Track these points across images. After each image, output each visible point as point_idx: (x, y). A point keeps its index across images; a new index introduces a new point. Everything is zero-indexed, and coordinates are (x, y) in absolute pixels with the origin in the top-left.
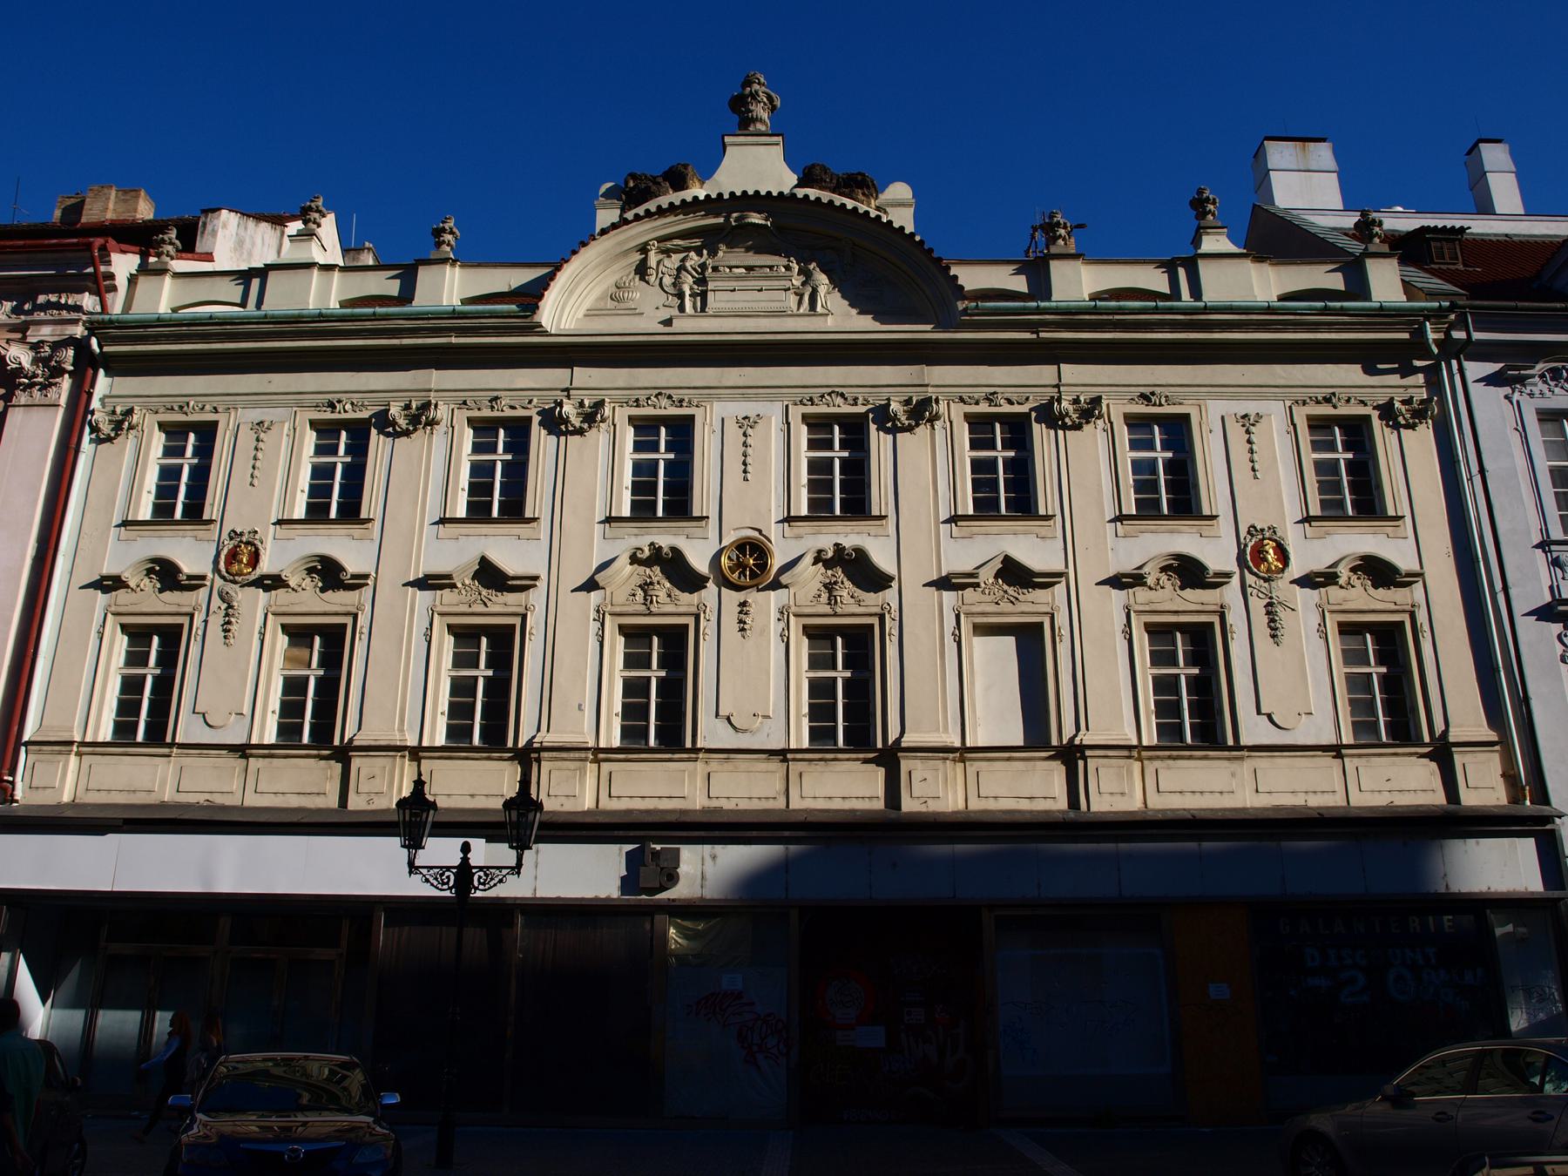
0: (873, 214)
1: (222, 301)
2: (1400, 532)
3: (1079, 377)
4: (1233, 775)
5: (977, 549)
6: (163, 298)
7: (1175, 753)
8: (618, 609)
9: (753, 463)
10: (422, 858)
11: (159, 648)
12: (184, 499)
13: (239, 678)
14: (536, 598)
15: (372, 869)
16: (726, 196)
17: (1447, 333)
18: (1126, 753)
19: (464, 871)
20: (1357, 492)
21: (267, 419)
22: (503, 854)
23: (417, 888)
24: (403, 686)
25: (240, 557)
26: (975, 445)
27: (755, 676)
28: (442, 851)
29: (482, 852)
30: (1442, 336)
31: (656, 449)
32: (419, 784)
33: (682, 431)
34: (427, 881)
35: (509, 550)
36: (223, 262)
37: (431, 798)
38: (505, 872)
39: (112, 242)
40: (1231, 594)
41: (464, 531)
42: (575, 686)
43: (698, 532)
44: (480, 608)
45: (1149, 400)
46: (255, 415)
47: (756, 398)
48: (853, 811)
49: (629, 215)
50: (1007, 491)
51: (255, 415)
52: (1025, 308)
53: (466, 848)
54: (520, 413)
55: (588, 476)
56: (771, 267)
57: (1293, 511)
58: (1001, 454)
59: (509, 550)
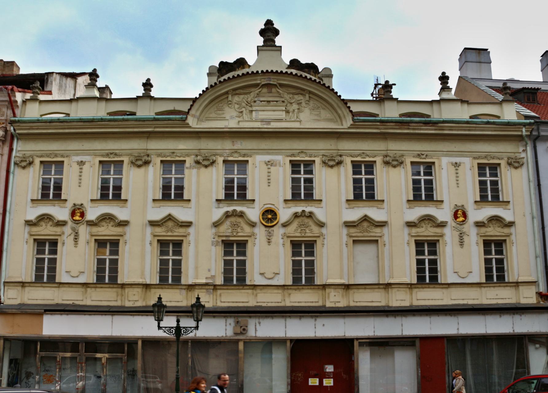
0: (318, 80)
1: (56, 113)
2: (508, 207)
5: (355, 214)
6: (32, 112)
8: (221, 234)
9: (269, 180)
10: (162, 324)
11: (46, 247)
12: (51, 192)
13: (76, 260)
14: (191, 230)
15: (145, 328)
16: (260, 72)
17: (531, 132)
18: (406, 286)
19: (178, 329)
20: (490, 193)
21: (84, 160)
22: (191, 323)
23: (161, 334)
24: (138, 262)
26: (413, 175)
27: (268, 259)
28: (170, 321)
29: (187, 322)
30: (529, 133)
32: (160, 299)
33: (429, 168)
34: (165, 332)
35: (180, 212)
36: (55, 96)
37: (203, 303)
38: (192, 329)
39: (15, 88)
40: (67, 230)
41: (162, 204)
42: (202, 261)
43: (251, 206)
44: (169, 234)
46: (79, 158)
49: (222, 79)
50: (364, 192)
51: (268, 158)
52: (375, 120)
54: (312, 159)
55: (205, 185)
56: (277, 101)
57: (471, 201)
59: (180, 212)
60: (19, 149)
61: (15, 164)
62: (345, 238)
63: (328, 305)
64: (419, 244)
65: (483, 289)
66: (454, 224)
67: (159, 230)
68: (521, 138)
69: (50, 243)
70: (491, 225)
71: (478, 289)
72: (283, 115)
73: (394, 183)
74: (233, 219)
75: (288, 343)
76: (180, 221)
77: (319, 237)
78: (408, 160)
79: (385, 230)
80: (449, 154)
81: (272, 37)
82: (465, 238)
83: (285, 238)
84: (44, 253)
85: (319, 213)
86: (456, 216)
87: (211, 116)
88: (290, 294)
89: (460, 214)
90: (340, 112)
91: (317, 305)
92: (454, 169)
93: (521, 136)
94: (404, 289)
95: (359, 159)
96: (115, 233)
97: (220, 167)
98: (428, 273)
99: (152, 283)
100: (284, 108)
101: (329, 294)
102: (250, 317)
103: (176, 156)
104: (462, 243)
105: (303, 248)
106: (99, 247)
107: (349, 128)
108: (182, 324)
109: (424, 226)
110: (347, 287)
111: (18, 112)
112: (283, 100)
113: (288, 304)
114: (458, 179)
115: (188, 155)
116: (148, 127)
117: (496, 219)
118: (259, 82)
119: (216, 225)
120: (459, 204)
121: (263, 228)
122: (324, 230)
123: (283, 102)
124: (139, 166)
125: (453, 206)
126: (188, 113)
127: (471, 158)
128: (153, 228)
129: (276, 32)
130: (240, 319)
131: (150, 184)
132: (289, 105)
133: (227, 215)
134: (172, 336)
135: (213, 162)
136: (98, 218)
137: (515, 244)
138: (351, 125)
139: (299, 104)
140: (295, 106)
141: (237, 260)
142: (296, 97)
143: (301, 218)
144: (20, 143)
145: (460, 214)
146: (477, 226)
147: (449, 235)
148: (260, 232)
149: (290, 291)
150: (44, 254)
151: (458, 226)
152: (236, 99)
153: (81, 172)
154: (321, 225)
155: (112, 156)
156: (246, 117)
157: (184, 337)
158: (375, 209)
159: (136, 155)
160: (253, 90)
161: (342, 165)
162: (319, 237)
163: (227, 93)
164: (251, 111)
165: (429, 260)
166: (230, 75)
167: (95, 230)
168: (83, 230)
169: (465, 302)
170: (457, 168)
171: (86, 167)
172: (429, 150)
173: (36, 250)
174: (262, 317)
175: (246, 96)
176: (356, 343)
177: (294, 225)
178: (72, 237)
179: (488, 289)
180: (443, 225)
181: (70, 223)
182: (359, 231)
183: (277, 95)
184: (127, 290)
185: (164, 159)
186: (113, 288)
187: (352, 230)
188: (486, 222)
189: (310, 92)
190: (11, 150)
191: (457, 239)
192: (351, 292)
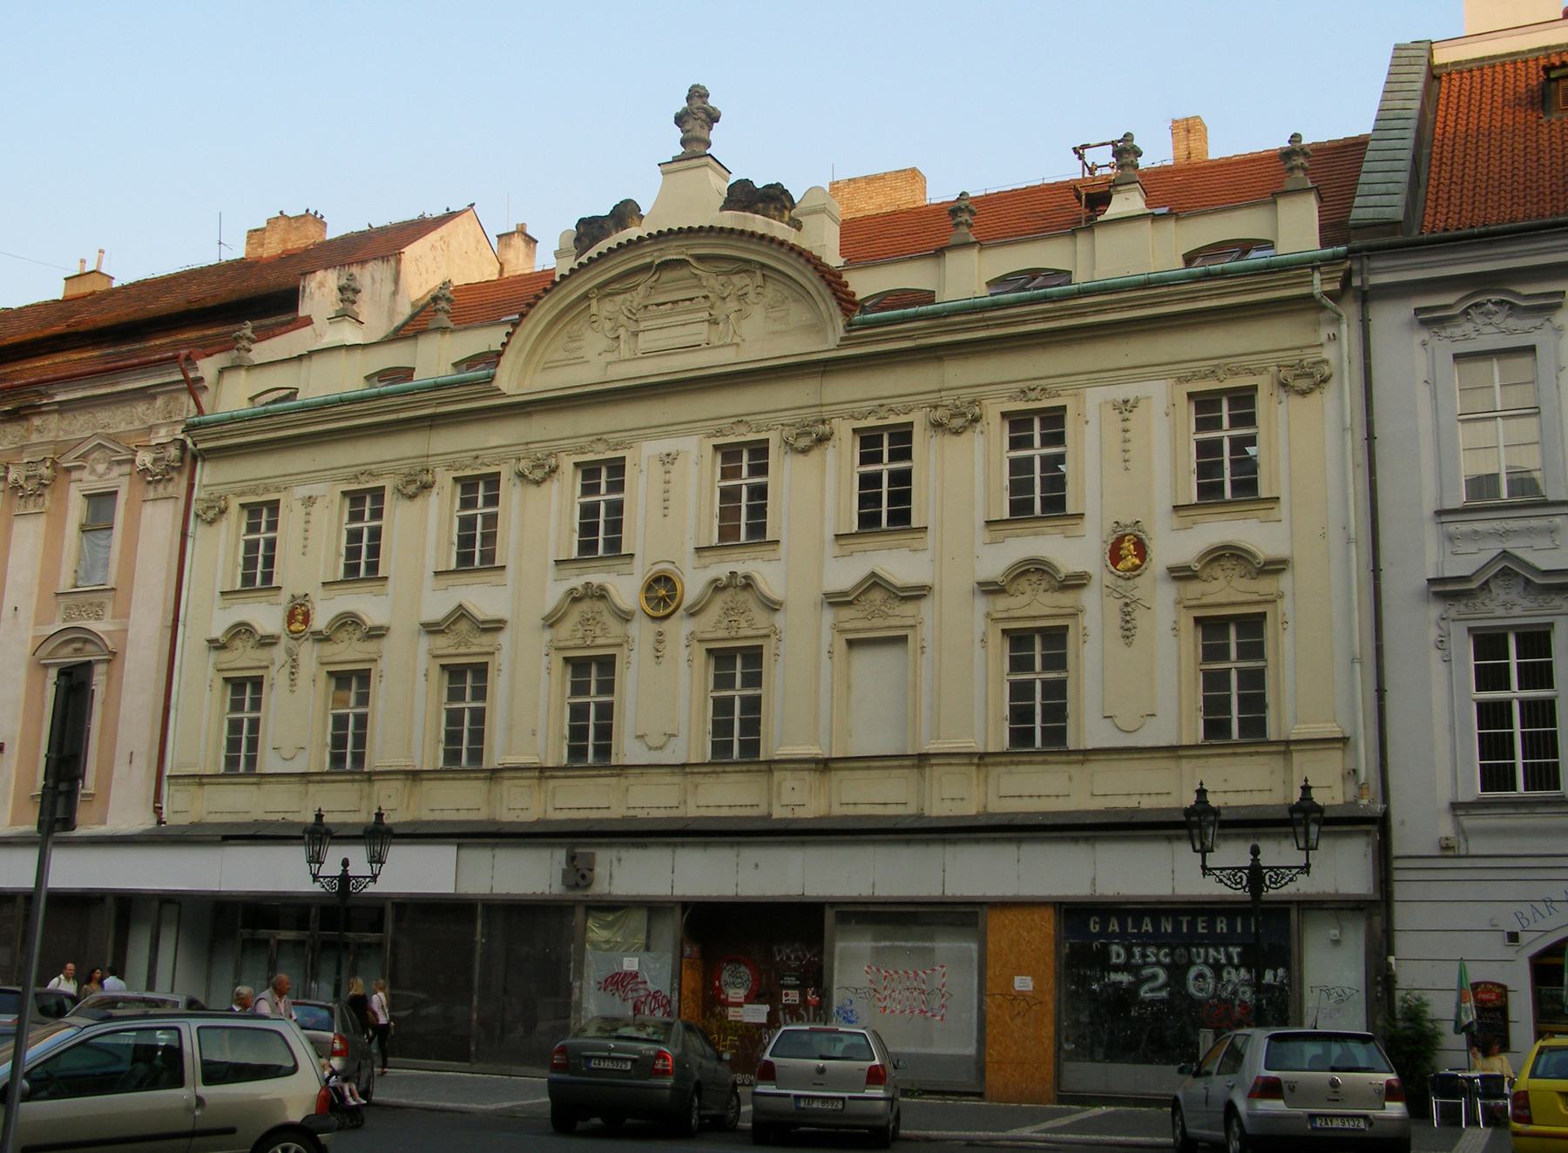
2: (1274, 514)
3: (959, 375)
4: (1070, 779)
7: (1253, 749)
8: (562, 644)
10: (1213, 860)
14: (503, 638)
15: (283, 872)
18: (966, 761)
19: (1256, 875)
20: (1226, 477)
23: (1211, 888)
25: (662, 589)
27: (662, 702)
29: (1278, 853)
31: (1219, 427)
40: (279, 654)
41: (450, 582)
43: (625, 569)
44: (462, 650)
45: (370, 474)
46: (303, 491)
47: (676, 434)
48: (588, 820)
49: (584, 259)
50: (886, 506)
53: (1255, 851)
54: (762, 436)
57: (1163, 505)
58: (745, 480)
60: (205, 482)
61: (197, 516)
62: (827, 636)
63: (779, 813)
64: (1019, 640)
65: (1184, 762)
66: (1109, 579)
67: (442, 643)
68: (1307, 304)
69: (744, 658)
70: (1218, 573)
71: (1172, 764)
72: (701, 332)
73: (960, 477)
74: (584, 606)
75: (678, 912)
76: (481, 617)
77: (767, 636)
78: (992, 411)
79: (926, 608)
80: (1098, 376)
81: (703, 134)
82: (1139, 615)
83: (552, 651)
84: (1225, 656)
85: (767, 572)
86: (1115, 555)
87: (556, 356)
88: (697, 786)
89: (1127, 549)
90: (822, 307)
91: (900, 810)
92: (662, 469)
93: (1310, 297)
94: (963, 769)
95: (871, 422)
96: (363, 656)
97: (1000, 434)
98: (1038, 723)
99: (425, 768)
100: (705, 315)
101: (779, 784)
102: (600, 845)
103: (483, 464)
104: (1127, 631)
105: (737, 664)
106: (338, 687)
107: (840, 347)
108: (1266, 860)
109: (1028, 589)
110: (824, 765)
111: (205, 399)
112: (705, 293)
113: (692, 812)
114: (1128, 446)
115: (505, 460)
116: (423, 407)
117: (1232, 555)
118: (648, 260)
119: (552, 621)
120: (1126, 519)
121: (647, 622)
122: (779, 619)
123: (706, 297)
124: (412, 497)
125: (1109, 525)
126: (499, 354)
127: (1171, 381)
128: (432, 637)
129: (713, 117)
130: (578, 850)
131: (432, 537)
132: (719, 303)
133: (575, 598)
134: (1242, 894)
135: (553, 470)
136: (330, 625)
137: (1290, 626)
138: (842, 339)
139: (742, 297)
140: (732, 305)
141: (1240, 671)
142: (736, 279)
143: (731, 591)
144: (208, 466)
145: (1127, 549)
146: (986, 593)
147: (1094, 615)
148: (642, 631)
149: (699, 779)
150: (1226, 658)
151: (1121, 582)
152: (608, 307)
153: (307, 522)
154: (773, 606)
155: (363, 478)
156: (625, 351)
157: (1271, 893)
158: (905, 551)
159: (406, 471)
160: (641, 278)
161: (831, 443)
162: (767, 636)
163: (585, 297)
164: (636, 334)
165: (1045, 683)
166: (603, 246)
167: (329, 651)
168: (309, 654)
169: (1131, 803)
170: (1127, 414)
171: (317, 510)
172: (1052, 373)
173: (568, 685)
174: (625, 845)
175: (628, 296)
176: (829, 916)
177: (715, 611)
178: (287, 669)
179: (1201, 762)
180: (1076, 582)
181: (284, 640)
182: (861, 615)
183: (694, 282)
184: (377, 785)
185: (460, 474)
186: (354, 781)
187: (846, 613)
188: (1198, 567)
189: (763, 266)
190: (191, 486)
191: (1115, 620)
192: (836, 777)
